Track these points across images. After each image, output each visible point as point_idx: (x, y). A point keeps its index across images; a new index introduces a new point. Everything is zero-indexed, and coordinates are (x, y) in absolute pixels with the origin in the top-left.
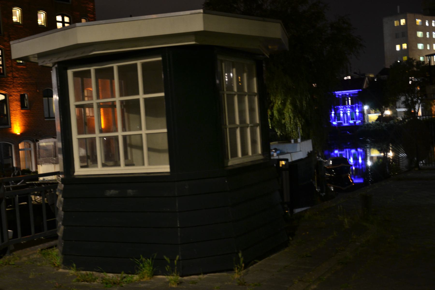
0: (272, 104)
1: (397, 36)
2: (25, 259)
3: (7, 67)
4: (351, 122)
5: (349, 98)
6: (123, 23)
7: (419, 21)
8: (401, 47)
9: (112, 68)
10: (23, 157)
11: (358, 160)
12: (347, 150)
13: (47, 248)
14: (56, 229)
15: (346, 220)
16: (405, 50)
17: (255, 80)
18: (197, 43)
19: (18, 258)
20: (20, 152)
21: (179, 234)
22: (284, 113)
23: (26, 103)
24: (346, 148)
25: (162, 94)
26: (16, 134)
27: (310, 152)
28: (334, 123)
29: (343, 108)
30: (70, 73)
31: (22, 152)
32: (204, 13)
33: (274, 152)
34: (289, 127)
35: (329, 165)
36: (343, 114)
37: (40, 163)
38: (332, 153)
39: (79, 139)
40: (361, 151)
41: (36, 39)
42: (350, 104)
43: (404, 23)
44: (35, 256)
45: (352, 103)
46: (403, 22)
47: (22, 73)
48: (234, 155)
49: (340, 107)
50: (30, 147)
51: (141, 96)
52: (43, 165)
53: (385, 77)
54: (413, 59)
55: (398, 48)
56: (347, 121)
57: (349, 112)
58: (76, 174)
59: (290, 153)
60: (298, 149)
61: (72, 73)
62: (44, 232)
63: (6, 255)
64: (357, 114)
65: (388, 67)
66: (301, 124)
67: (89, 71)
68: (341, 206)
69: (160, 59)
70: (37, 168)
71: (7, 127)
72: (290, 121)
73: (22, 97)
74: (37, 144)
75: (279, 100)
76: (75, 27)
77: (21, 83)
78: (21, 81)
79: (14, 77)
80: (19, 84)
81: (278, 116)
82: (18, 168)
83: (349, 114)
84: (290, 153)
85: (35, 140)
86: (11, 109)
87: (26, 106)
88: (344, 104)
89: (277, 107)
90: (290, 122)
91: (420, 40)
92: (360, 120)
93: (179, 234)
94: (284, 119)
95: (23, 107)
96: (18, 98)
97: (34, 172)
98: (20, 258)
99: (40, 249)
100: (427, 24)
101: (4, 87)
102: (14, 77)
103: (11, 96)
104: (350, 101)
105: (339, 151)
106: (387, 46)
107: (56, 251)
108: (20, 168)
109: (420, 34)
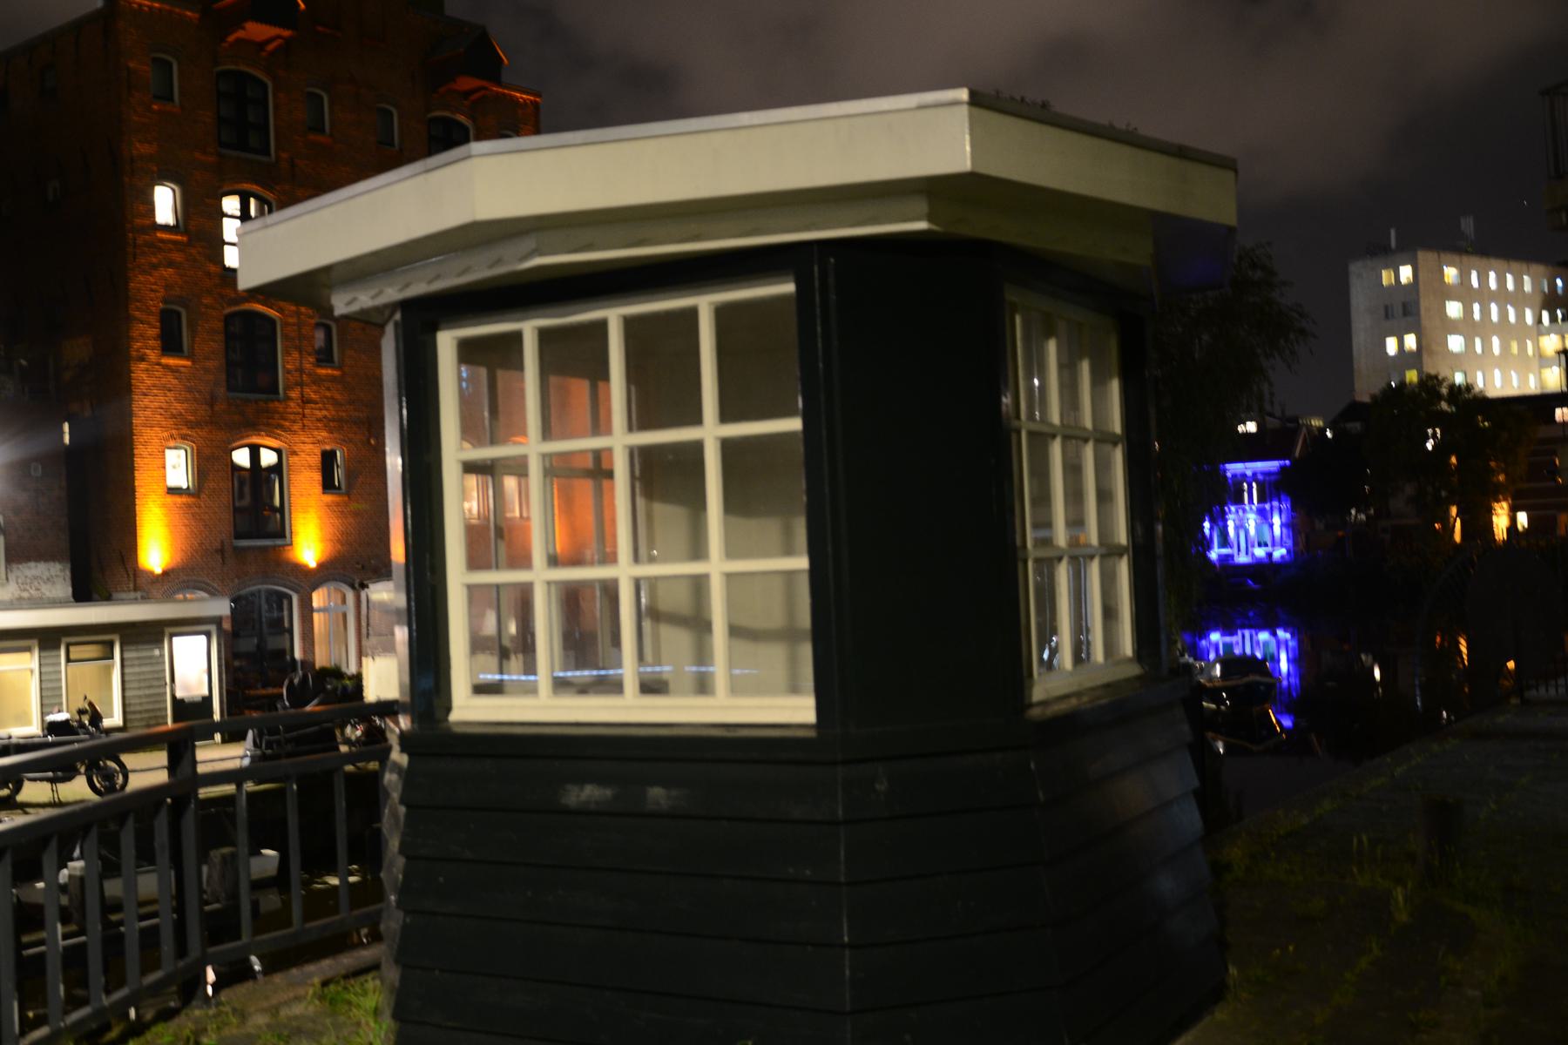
1: (1388, 313)
2: (261, 1020)
3: (288, 372)
5: (1254, 485)
6: (652, 143)
7: (1451, 274)
9: (601, 327)
10: (323, 630)
12: (1247, 633)
13: (346, 977)
14: (378, 906)
15: (1399, 894)
16: (1411, 353)
17: (1115, 386)
18: (934, 227)
19: (234, 1020)
20: (316, 616)
21: (847, 972)
23: (339, 475)
24: (1243, 627)
25: (794, 424)
26: (306, 566)
30: (447, 342)
31: (319, 616)
35: (1211, 679)
36: (1237, 528)
37: (370, 653)
39: (471, 589)
40: (1288, 636)
41: (326, 213)
44: (297, 1009)
45: (1261, 500)
46: (1406, 273)
47: (328, 389)
50: (344, 601)
51: (711, 432)
52: (378, 659)
53: (1355, 426)
54: (1440, 378)
55: (1391, 346)
56: (1247, 548)
58: (455, 716)
62: (337, 918)
63: (194, 1003)
67: (517, 337)
68: (1365, 838)
69: (789, 288)
70: (360, 664)
71: (279, 542)
73: (328, 459)
74: (363, 595)
76: (469, 157)
77: (325, 417)
78: (325, 413)
79: (305, 401)
80: (319, 420)
82: (308, 664)
83: (1252, 532)
85: (357, 586)
86: (293, 490)
87: (337, 484)
88: (1239, 501)
91: (1453, 327)
92: (1282, 546)
93: (847, 972)
95: (328, 485)
96: (316, 460)
97: (351, 678)
98: (243, 1016)
99: (316, 980)
100: (1475, 282)
101: (276, 428)
102: (305, 401)
103: (294, 453)
105: (1223, 635)
106: (1360, 338)
107: (372, 997)
108: (313, 664)
109: (1454, 309)
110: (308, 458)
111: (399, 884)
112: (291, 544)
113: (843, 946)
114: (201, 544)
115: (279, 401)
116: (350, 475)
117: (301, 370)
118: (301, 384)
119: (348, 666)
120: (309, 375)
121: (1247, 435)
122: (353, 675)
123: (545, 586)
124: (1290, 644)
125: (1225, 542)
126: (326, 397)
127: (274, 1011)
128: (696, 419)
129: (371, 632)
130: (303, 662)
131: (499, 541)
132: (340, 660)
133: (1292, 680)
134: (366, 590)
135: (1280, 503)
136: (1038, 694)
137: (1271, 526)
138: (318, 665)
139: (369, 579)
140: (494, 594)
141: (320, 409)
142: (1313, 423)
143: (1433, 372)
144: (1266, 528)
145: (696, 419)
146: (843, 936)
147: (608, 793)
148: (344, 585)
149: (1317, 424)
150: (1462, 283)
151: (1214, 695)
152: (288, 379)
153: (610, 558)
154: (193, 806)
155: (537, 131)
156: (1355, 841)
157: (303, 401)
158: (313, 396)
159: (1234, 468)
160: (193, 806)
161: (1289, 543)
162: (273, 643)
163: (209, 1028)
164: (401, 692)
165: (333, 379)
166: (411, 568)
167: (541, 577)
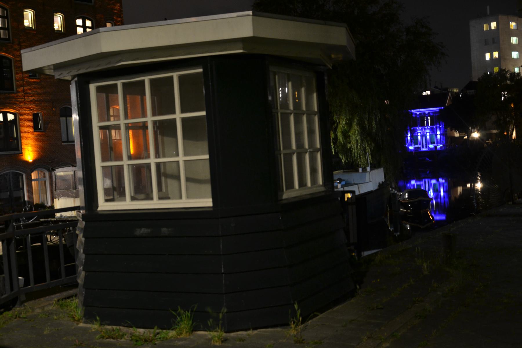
0: (336, 125)
1: (486, 43)
2: (38, 311)
3: (18, 81)
4: (431, 146)
5: (429, 118)
8: (492, 55)
10: (36, 189)
11: (440, 192)
14: (75, 276)
16: (496, 59)
17: (315, 95)
19: (31, 311)
21: (224, 281)
22: (350, 136)
23: (40, 123)
24: (425, 178)
25: (204, 113)
27: (381, 183)
28: (411, 148)
29: (422, 129)
30: (92, 88)
32: (254, 15)
33: (338, 183)
34: (356, 153)
35: (404, 199)
36: (422, 136)
38: (407, 183)
40: (444, 181)
42: (429, 125)
43: (495, 27)
44: (51, 308)
46: (494, 25)
47: (35, 88)
48: (290, 185)
49: (417, 128)
50: (45, 177)
51: (178, 116)
52: (60, 199)
53: (471, 92)
55: (488, 56)
56: (426, 145)
57: (428, 134)
58: (99, 209)
59: (358, 184)
60: (367, 180)
61: (95, 87)
63: (16, 306)
64: (439, 136)
65: (476, 79)
66: (370, 149)
67: (116, 86)
69: (201, 70)
70: (53, 202)
71: (17, 152)
72: (357, 145)
73: (35, 117)
74: (53, 173)
75: (343, 120)
77: (34, 99)
79: (25, 93)
81: (343, 139)
82: (31, 202)
83: (428, 137)
84: (358, 184)
86: (22, 131)
88: (422, 125)
89: (341, 129)
90: (357, 147)
93: (224, 281)
94: (350, 143)
95: (36, 128)
96: (30, 118)
97: (49, 207)
98: (33, 310)
101: (14, 105)
102: (25, 93)
103: (22, 115)
104: (429, 121)
110: (27, 117)
111: (83, 263)
112: (22, 153)
113: (222, 273)
114: (38, 157)
115: (14, 93)
116: (45, 123)
117: (23, 80)
118: (23, 86)
119: (47, 203)
120: (26, 82)
121: (427, 96)
122: (49, 206)
123: (127, 166)
124: (445, 184)
125: (416, 142)
126: (34, 91)
127: (43, 308)
128: (174, 112)
129: (57, 189)
130: (28, 201)
131: (112, 152)
132: (44, 201)
133: (446, 199)
134: (55, 171)
135: (440, 125)
136: (285, 196)
137: (436, 135)
138: (35, 203)
139: (55, 167)
140: (110, 169)
141: (32, 96)
142: (454, 91)
143: (504, 68)
144: (434, 136)
145: (174, 112)
146: (222, 271)
147: (149, 230)
148: (45, 170)
149: (456, 91)
150: (517, 29)
151: (405, 206)
152: (17, 84)
153: (148, 157)
154: (13, 242)
155: (122, 24)
156: (416, 248)
157: (24, 93)
158: (28, 91)
159: (416, 111)
160: (13, 242)
161: (444, 141)
162: (16, 194)
163: (22, 313)
164: (81, 203)
165: (37, 83)
166: (84, 161)
167: (125, 163)
